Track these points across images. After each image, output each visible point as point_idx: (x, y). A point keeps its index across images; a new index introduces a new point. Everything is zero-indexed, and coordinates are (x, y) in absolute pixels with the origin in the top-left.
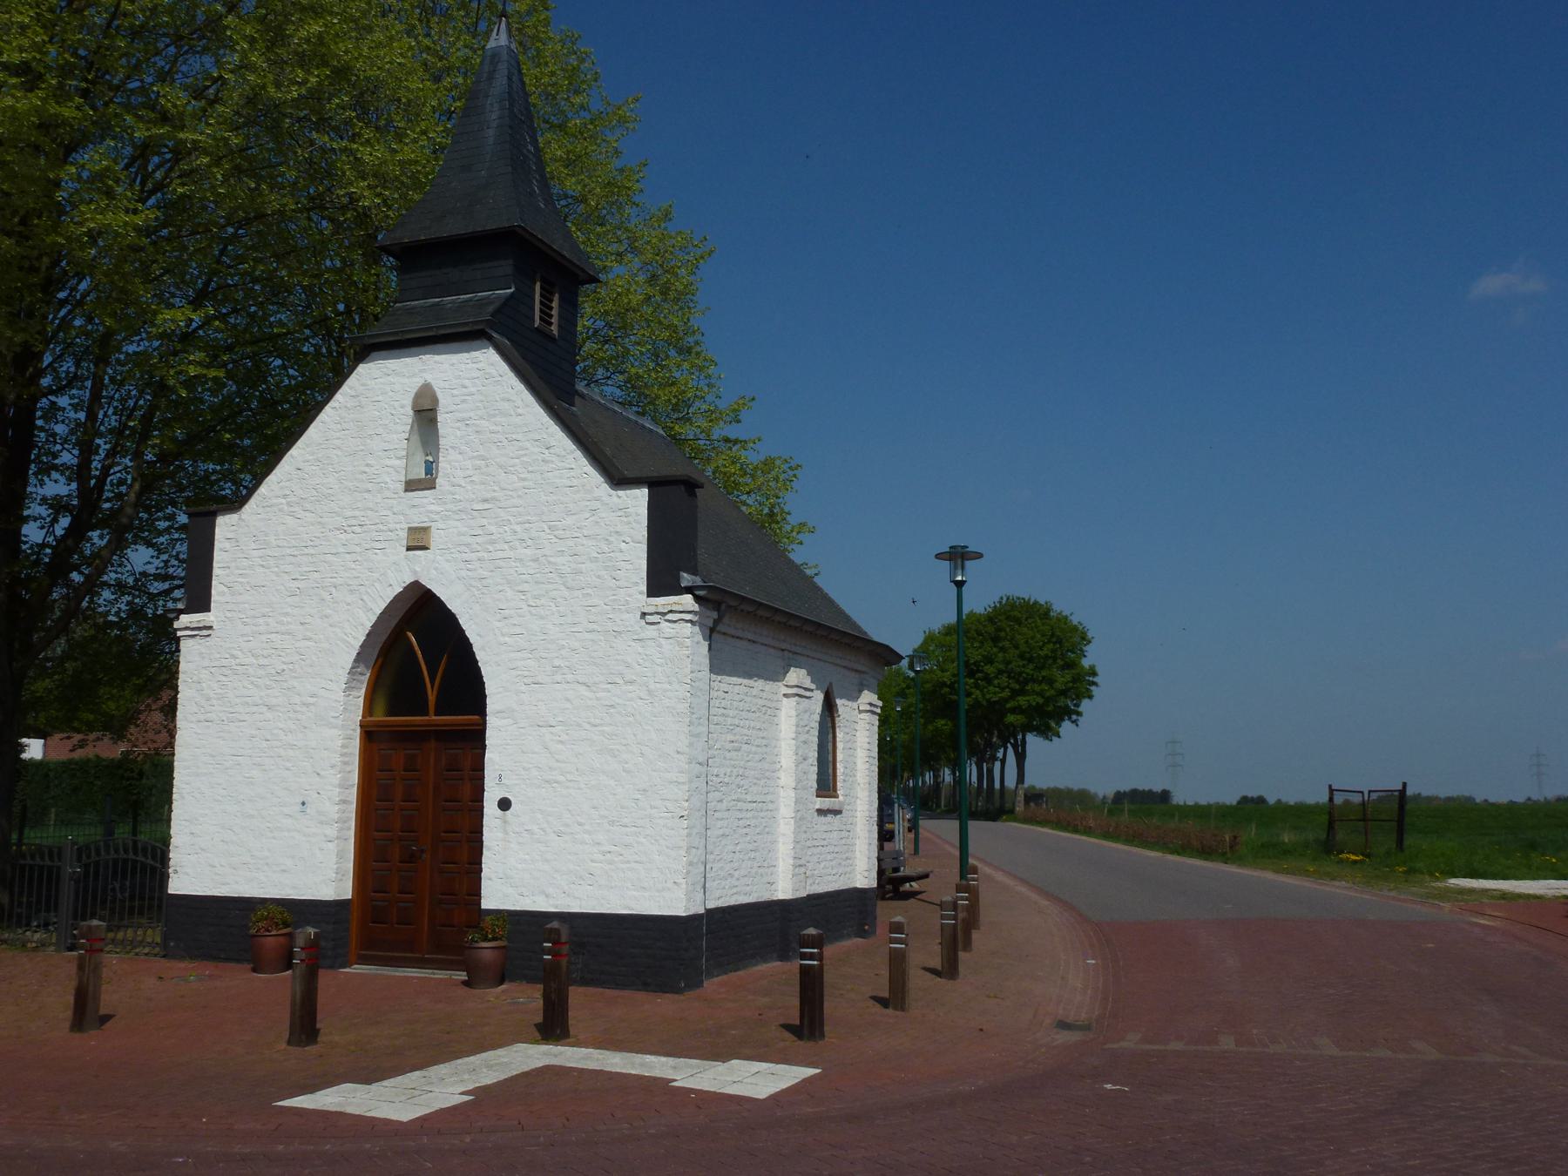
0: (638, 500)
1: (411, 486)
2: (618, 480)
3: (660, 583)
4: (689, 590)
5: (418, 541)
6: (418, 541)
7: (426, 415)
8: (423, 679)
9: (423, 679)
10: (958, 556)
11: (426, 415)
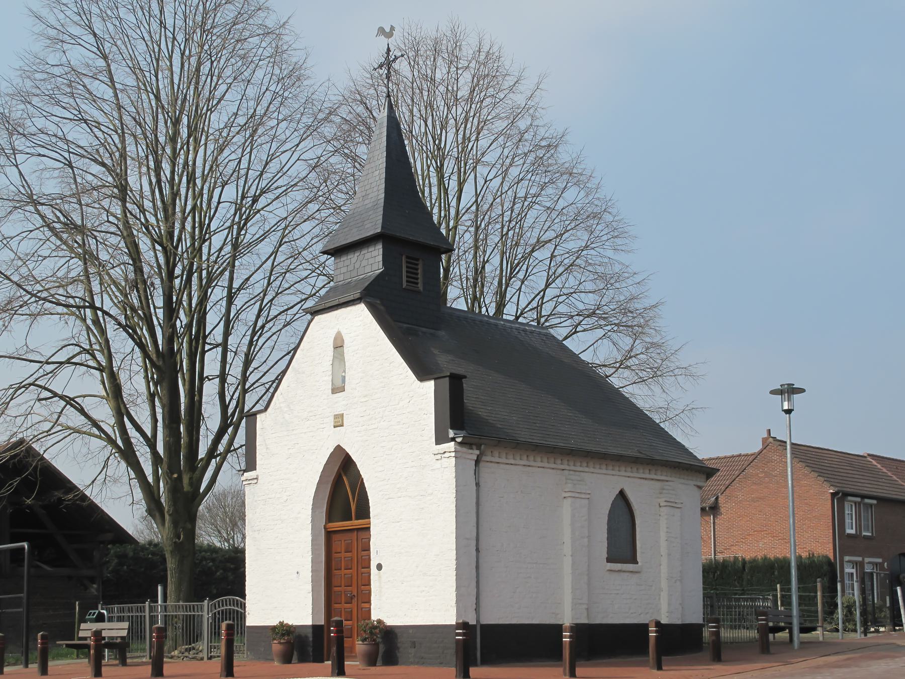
0: (430, 385)
1: (335, 391)
2: (422, 372)
3: (441, 438)
4: (453, 439)
5: (339, 421)
6: (339, 421)
7: (339, 345)
8: (343, 496)
9: (343, 496)
10: (789, 391)
11: (339, 345)
